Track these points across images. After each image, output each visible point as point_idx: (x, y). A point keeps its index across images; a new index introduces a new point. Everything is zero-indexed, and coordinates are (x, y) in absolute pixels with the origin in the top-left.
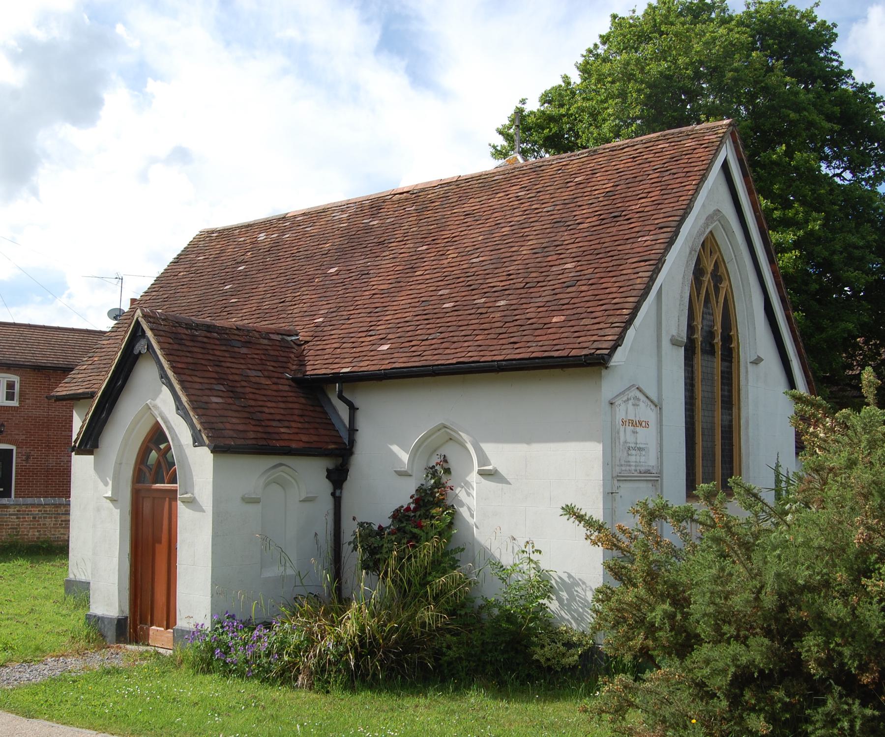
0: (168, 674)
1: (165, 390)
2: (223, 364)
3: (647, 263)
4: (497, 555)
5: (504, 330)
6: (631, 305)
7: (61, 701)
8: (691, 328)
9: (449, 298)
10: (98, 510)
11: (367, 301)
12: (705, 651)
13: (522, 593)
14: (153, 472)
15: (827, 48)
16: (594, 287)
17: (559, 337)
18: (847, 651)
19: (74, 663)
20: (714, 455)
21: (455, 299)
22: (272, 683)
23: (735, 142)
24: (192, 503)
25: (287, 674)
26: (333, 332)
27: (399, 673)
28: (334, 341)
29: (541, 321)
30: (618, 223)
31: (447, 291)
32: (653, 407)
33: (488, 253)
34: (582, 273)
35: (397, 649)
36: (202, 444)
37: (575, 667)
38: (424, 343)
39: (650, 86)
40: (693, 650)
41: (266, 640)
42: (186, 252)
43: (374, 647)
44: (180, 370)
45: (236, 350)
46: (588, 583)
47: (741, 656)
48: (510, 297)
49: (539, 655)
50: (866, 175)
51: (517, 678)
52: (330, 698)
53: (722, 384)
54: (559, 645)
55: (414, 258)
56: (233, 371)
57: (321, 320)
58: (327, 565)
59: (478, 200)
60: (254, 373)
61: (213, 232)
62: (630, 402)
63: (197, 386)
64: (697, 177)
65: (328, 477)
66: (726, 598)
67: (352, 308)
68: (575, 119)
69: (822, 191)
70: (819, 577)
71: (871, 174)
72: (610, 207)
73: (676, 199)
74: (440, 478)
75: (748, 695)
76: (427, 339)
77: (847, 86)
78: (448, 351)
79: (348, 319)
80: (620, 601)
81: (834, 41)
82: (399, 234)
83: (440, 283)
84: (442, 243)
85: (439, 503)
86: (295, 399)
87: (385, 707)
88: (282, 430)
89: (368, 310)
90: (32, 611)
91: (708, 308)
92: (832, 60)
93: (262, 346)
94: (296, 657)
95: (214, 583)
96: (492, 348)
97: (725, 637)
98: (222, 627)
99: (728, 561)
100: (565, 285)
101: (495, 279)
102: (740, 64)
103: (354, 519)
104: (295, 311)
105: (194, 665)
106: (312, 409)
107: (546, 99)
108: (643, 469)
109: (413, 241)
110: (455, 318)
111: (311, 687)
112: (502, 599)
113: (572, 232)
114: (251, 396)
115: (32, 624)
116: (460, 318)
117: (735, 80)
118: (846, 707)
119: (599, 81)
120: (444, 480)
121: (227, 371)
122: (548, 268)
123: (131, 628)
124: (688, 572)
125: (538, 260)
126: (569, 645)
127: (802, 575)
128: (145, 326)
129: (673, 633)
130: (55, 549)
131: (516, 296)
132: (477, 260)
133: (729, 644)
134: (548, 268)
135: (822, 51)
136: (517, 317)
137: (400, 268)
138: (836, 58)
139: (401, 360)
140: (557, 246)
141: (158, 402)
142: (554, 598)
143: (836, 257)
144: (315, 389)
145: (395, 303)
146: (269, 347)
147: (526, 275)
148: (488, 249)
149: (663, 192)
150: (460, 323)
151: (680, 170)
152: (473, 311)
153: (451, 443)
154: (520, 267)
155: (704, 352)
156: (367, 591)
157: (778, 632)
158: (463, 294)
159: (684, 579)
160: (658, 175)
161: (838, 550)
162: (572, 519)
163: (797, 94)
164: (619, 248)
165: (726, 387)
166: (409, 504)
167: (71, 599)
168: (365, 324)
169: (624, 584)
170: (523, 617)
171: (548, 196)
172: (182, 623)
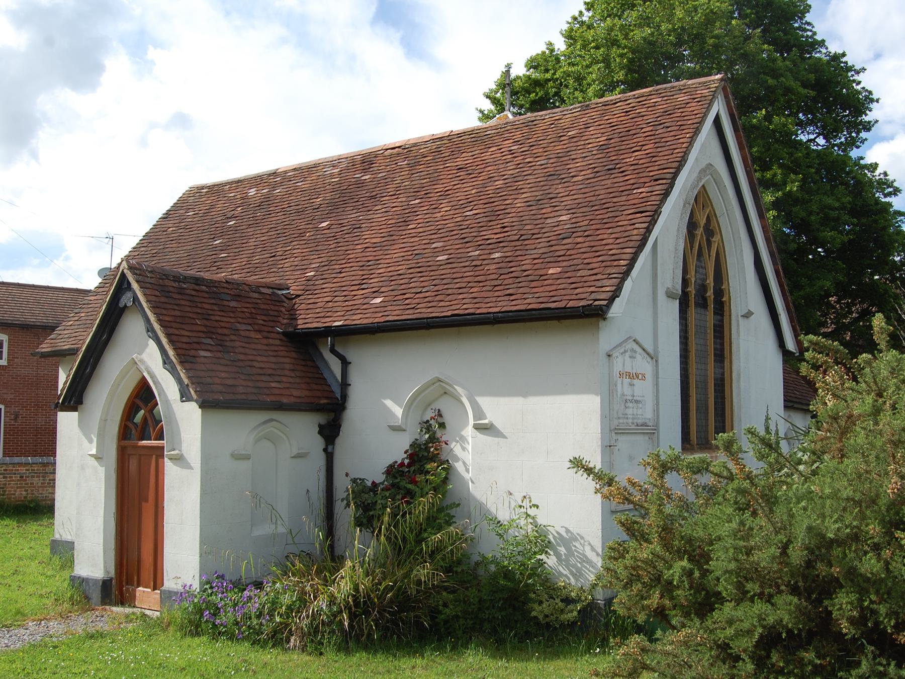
0: (155, 637)
1: (152, 344)
2: (212, 317)
3: (643, 215)
4: (493, 510)
5: (499, 282)
6: (628, 256)
7: (40, 669)
8: (685, 282)
9: (443, 251)
10: (83, 468)
11: (360, 255)
12: (728, 609)
13: (520, 548)
14: (139, 429)
15: (801, 19)
16: (589, 239)
17: (555, 288)
18: (883, 609)
19: (56, 627)
20: (707, 409)
21: (449, 252)
22: (263, 645)
23: (726, 97)
24: (179, 459)
25: (279, 636)
26: (324, 286)
27: (394, 633)
28: (325, 295)
29: (537, 272)
30: (613, 176)
31: (441, 244)
32: (649, 359)
33: (481, 206)
34: (578, 225)
35: (392, 608)
36: (189, 399)
37: (574, 623)
38: (417, 296)
39: (633, 52)
40: (714, 610)
41: (258, 600)
42: (176, 207)
43: (368, 606)
44: (167, 324)
45: (226, 303)
46: (587, 538)
47: (767, 615)
48: (505, 250)
49: (537, 611)
50: (838, 141)
51: (515, 635)
52: (323, 659)
53: (715, 337)
54: (558, 601)
55: (407, 211)
56: (223, 324)
57: (312, 273)
58: (319, 522)
59: (470, 154)
60: (244, 327)
61: (203, 188)
62: (627, 354)
63: (185, 340)
64: (691, 131)
65: (320, 433)
66: (748, 554)
67: (344, 262)
68: (561, 84)
69: (800, 154)
70: (848, 530)
71: (843, 140)
72: (604, 160)
73: (670, 152)
74: (435, 433)
75: (775, 657)
76: (420, 292)
77: (820, 55)
78: (442, 304)
79: (340, 273)
80: (634, 558)
81: (808, 11)
82: (391, 188)
83: (433, 236)
84: (434, 197)
85: (433, 458)
86: (285, 354)
87: (380, 669)
88: (273, 385)
89: (361, 264)
90: (16, 572)
91: (700, 262)
92: (806, 30)
93: (251, 301)
94: (288, 618)
95: (202, 542)
96: (487, 300)
97: (749, 595)
98: (211, 588)
99: (747, 514)
100: (561, 237)
101: (490, 232)
102: (720, 31)
103: (347, 475)
104: (286, 265)
105: (181, 628)
106: (303, 363)
107: (533, 64)
108: (640, 421)
109: (405, 195)
110: (449, 271)
111: (303, 649)
112: (499, 555)
113: (566, 184)
114: (241, 350)
115: (14, 586)
116: (454, 271)
117: (716, 47)
118: (882, 669)
119: (584, 47)
120: (438, 435)
121: (216, 324)
122: (542, 221)
123: (117, 589)
124: (705, 527)
125: (532, 213)
126: (568, 601)
127: (831, 529)
128: (130, 278)
129: (692, 592)
130: (39, 508)
131: (512, 249)
132: (471, 213)
133: (753, 602)
134: (542, 221)
135: (796, 21)
136: (512, 269)
137: (393, 221)
138: (809, 28)
139: (395, 313)
140: (551, 198)
141: (144, 356)
142: (552, 553)
143: (813, 218)
144: (306, 344)
145: (387, 257)
146: (259, 301)
147: (520, 227)
148: (481, 202)
149: (656, 145)
150: (454, 276)
151: (673, 124)
152: (467, 264)
153: (445, 396)
154: (514, 219)
155: (697, 305)
156: (361, 549)
157: (805, 589)
158: (457, 247)
159: (700, 533)
160: (651, 128)
161: (866, 503)
162: (581, 472)
163: (774, 60)
164: (615, 200)
165: (718, 341)
166: (403, 459)
167: (56, 560)
168: (357, 277)
169: (637, 540)
170: (521, 574)
171: (541, 150)
172: (170, 583)
